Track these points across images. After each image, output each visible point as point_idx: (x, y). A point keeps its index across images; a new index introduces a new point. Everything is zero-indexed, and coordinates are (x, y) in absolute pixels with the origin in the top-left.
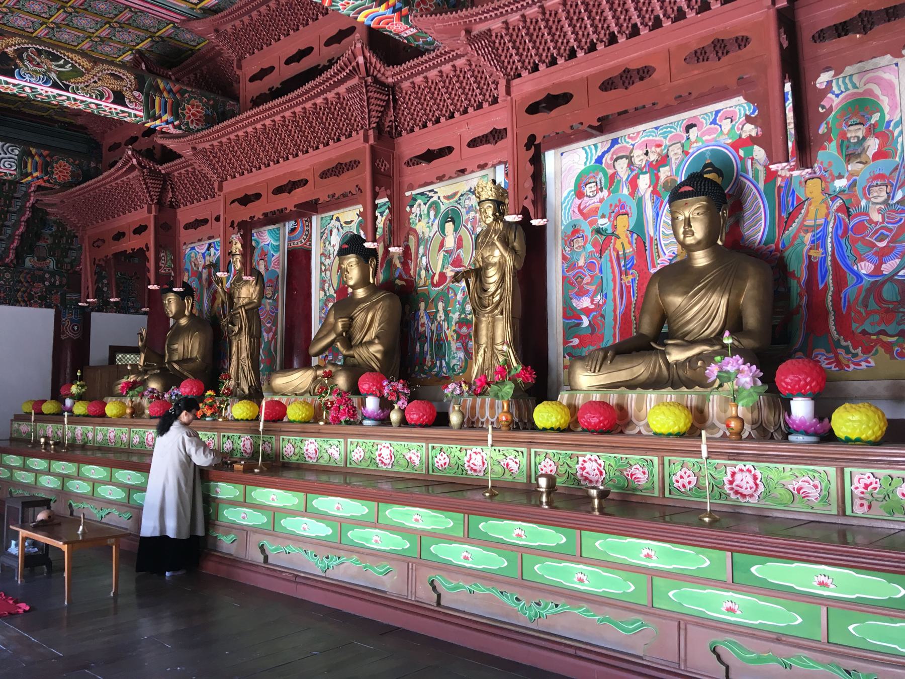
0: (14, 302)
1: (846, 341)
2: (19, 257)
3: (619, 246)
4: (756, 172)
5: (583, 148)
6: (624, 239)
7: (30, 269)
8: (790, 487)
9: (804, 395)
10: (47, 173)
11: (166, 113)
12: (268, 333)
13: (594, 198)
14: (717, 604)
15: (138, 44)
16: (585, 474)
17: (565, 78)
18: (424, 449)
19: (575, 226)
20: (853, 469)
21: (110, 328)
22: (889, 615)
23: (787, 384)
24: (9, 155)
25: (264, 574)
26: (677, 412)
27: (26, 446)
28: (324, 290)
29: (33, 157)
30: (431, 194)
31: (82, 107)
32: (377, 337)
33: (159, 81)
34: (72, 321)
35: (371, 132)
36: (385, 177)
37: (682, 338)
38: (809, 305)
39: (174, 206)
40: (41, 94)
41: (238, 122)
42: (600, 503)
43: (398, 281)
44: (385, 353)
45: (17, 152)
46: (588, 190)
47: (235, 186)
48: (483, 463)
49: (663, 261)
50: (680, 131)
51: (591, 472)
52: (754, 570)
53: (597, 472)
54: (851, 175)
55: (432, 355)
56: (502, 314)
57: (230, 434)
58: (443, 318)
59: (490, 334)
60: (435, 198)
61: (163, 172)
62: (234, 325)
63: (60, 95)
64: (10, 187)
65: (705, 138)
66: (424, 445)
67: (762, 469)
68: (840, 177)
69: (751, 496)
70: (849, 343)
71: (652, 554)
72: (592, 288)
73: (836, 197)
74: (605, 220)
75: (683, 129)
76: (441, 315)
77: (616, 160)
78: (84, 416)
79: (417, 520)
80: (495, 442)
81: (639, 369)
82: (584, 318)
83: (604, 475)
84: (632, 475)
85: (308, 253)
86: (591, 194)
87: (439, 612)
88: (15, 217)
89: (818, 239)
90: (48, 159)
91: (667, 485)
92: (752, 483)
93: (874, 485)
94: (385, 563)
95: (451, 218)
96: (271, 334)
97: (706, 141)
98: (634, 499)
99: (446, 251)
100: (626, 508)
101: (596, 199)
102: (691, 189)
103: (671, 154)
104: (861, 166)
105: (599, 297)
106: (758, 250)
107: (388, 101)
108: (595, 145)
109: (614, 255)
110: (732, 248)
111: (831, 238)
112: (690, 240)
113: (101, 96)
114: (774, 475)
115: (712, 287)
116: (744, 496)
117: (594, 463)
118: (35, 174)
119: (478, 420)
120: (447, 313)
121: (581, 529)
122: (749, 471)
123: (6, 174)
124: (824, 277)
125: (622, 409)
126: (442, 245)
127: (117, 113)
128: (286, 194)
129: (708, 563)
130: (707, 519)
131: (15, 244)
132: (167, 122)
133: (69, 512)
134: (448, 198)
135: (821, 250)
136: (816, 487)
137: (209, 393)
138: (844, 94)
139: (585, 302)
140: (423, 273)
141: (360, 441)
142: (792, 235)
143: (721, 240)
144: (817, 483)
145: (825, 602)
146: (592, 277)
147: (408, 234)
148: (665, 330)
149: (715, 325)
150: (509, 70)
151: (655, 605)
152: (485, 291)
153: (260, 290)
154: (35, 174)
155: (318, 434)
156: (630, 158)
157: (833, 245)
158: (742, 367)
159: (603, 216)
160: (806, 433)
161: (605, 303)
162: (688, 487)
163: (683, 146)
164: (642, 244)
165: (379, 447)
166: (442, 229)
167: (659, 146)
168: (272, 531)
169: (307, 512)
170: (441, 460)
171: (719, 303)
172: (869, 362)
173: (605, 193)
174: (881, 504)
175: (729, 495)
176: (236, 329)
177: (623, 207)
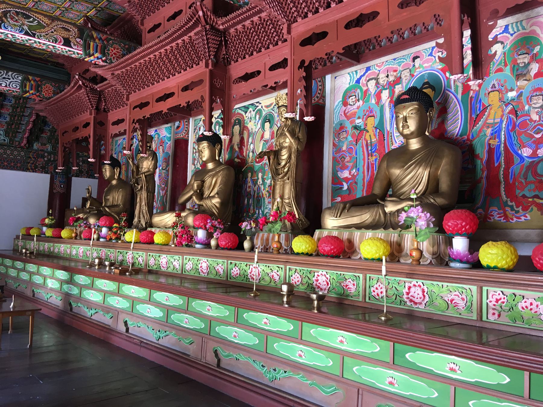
0: (26, 169)
1: (511, 202)
2: (30, 143)
3: (368, 137)
4: (456, 87)
5: (349, 73)
6: (371, 132)
7: (36, 150)
8: (446, 299)
9: (461, 235)
10: (38, 91)
11: (97, 52)
12: (163, 190)
13: (356, 106)
14: (383, 378)
15: (88, 12)
16: (318, 284)
17: (323, 22)
18: (226, 264)
19: (341, 124)
20: (489, 288)
21: (81, 187)
22: (497, 397)
23: (449, 226)
24: (15, 80)
25: (125, 339)
26: (378, 244)
27: (16, 254)
28: (194, 165)
29: (30, 81)
30: (257, 105)
31: (44, 47)
32: (217, 193)
33: (93, 33)
34: (60, 181)
35: (210, 61)
36: (221, 92)
37: (398, 197)
38: (488, 177)
39: (106, 111)
40: (18, 39)
41: (133, 56)
42: (318, 304)
43: (236, 160)
44: (222, 204)
45: (20, 78)
46: (350, 101)
47: (135, 97)
48: (259, 274)
49: (396, 145)
50: (409, 61)
51: (322, 283)
52: (407, 356)
53: (325, 283)
54: (519, 88)
55: (254, 206)
56: (288, 179)
57: (122, 251)
58: (261, 183)
59: (281, 192)
60: (260, 107)
61: (98, 89)
62: (138, 185)
63: (31, 40)
64: (23, 101)
65: (424, 65)
66: (361, 276)
67: (429, 285)
68: (512, 90)
69: (420, 303)
70: (514, 203)
71: (344, 340)
72: (350, 165)
73: (509, 103)
74: (360, 120)
75: (411, 59)
76: (260, 181)
77: (368, 81)
78: (51, 237)
79: (209, 310)
80: (260, 260)
81: (366, 217)
82: (345, 184)
83: (330, 285)
84: (346, 286)
85: (186, 142)
86: (352, 103)
87: (218, 369)
88: (27, 119)
89: (496, 132)
90: (39, 83)
91: (367, 294)
92: (421, 293)
93: (502, 300)
94: (190, 337)
95: (264, 118)
96: (164, 191)
97: (426, 67)
98: (346, 302)
99: (265, 141)
100: (340, 309)
101: (355, 107)
102: (408, 97)
103: (403, 76)
104: (526, 82)
105: (354, 171)
106: (456, 139)
107: (221, 41)
108: (356, 71)
109: (364, 143)
110: (435, 138)
111: (504, 131)
112: (406, 132)
113: (56, 41)
114: (436, 289)
115: (419, 164)
116: (416, 303)
117: (324, 277)
118: (31, 92)
119: (270, 247)
120: (263, 179)
121: (302, 321)
122: (420, 286)
123: (13, 91)
124: (498, 159)
125: (350, 242)
126: (262, 137)
127: (67, 52)
128: (163, 102)
129: (379, 349)
130: (383, 318)
131: (27, 135)
132: (98, 58)
133: (32, 295)
134: (267, 107)
135: (497, 140)
136: (463, 299)
137: (115, 225)
138: (516, 34)
139: (346, 174)
140: (251, 154)
141: (191, 257)
142: (478, 130)
143: (428, 132)
144: (464, 296)
145: (453, 383)
146: (351, 157)
147: (243, 130)
148: (390, 193)
149: (420, 188)
150: (290, 18)
151: (344, 376)
152: (279, 164)
153: (154, 163)
154: (31, 92)
155: (168, 252)
156: (377, 79)
157: (505, 136)
158: (420, 214)
159: (359, 118)
160: (461, 261)
161: (358, 174)
162: (380, 295)
163: (410, 71)
164: (382, 136)
165: (201, 261)
166: (263, 126)
167: (395, 71)
168: (132, 312)
169: (238, 323)
170: (235, 271)
171: (422, 174)
172: (526, 217)
173: (361, 102)
174: (507, 314)
175: (406, 302)
176: (139, 187)
177: (371, 112)
